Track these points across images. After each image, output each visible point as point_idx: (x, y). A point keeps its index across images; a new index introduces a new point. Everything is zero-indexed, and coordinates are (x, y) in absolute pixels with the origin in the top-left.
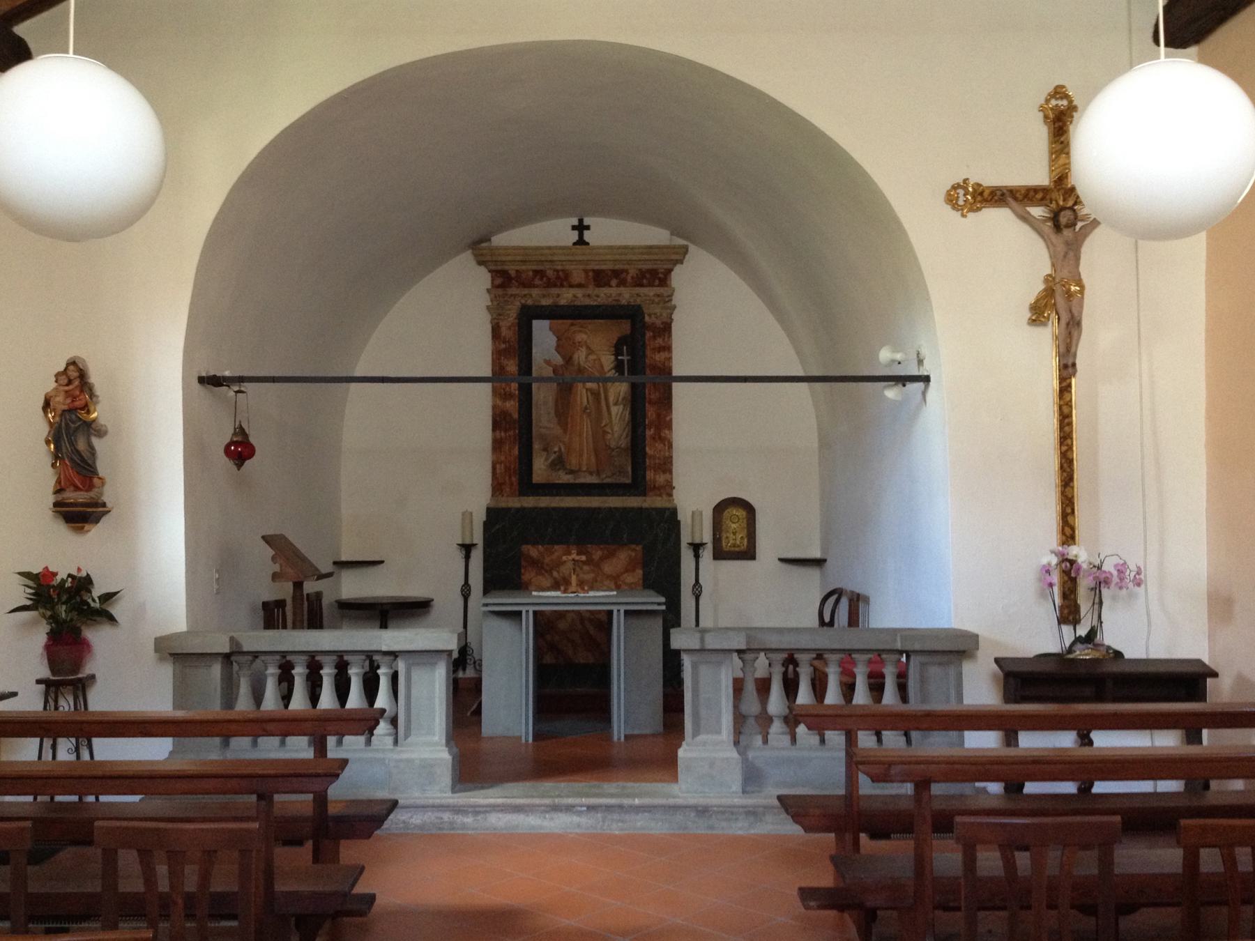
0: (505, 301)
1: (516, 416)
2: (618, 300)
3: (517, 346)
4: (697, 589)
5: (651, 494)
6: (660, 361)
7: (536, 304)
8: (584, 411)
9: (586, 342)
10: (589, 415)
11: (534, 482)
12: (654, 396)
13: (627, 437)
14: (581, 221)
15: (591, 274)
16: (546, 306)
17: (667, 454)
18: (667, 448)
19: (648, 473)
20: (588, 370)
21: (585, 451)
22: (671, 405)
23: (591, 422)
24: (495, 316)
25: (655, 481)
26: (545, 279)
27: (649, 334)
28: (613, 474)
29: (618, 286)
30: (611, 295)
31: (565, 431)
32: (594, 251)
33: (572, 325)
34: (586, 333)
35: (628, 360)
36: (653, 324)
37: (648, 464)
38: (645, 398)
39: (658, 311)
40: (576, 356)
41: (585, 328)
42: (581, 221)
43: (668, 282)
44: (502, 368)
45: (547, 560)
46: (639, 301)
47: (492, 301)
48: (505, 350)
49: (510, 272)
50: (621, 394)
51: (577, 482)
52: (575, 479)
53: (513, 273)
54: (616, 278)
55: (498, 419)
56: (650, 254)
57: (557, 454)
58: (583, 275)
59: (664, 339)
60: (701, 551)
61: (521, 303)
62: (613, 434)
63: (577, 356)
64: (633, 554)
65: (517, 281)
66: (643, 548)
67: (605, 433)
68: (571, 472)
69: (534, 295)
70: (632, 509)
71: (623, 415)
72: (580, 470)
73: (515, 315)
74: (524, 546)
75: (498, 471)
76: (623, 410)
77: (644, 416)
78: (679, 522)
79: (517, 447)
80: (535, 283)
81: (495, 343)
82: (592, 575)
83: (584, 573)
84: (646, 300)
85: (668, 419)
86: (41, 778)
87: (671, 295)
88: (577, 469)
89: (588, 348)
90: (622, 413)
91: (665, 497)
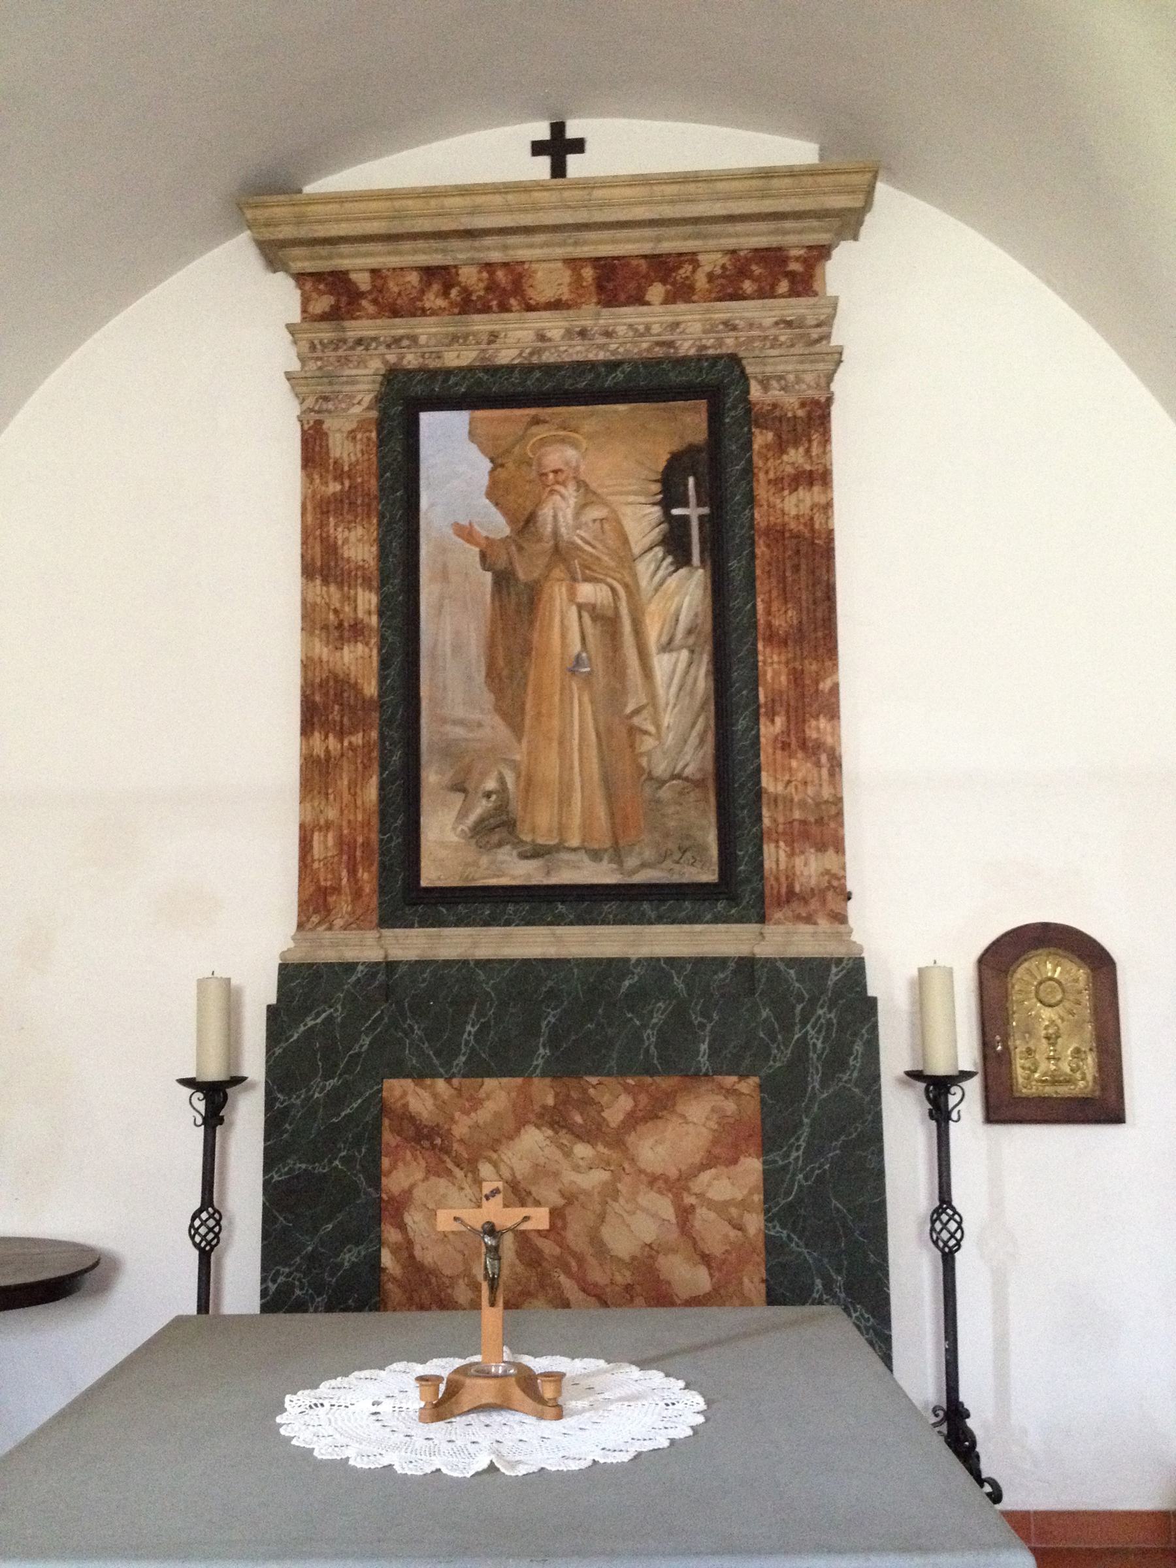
0: (339, 359)
1: (371, 689)
2: (670, 344)
3: (373, 485)
4: (945, 1226)
5: (778, 915)
6: (797, 517)
7: (433, 364)
8: (573, 672)
9: (576, 469)
10: (588, 679)
11: (424, 883)
12: (784, 619)
13: (702, 741)
14: (558, 129)
15: (588, 273)
16: (460, 369)
17: (826, 793)
18: (825, 772)
19: (768, 849)
20: (584, 551)
21: (578, 785)
22: (835, 647)
23: (592, 702)
24: (310, 402)
25: (791, 877)
26: (454, 292)
27: (762, 439)
28: (665, 856)
29: (669, 299)
30: (648, 328)
31: (517, 729)
32: (598, 193)
33: (536, 421)
34: (575, 445)
35: (701, 518)
36: (775, 406)
37: (766, 822)
38: (754, 625)
39: (787, 367)
40: (546, 512)
41: (575, 431)
42: (558, 129)
43: (816, 287)
44: (331, 549)
45: (461, 1128)
46: (730, 344)
47: (302, 359)
48: (338, 499)
49: (353, 276)
50: (682, 618)
51: (553, 881)
52: (548, 873)
53: (363, 281)
54: (664, 281)
55: (317, 698)
56: (764, 195)
57: (494, 797)
58: (566, 276)
59: (808, 451)
60: (952, 1100)
61: (385, 362)
62: (659, 736)
63: (551, 513)
64: (730, 1106)
65: (375, 302)
66: (761, 1087)
67: (634, 732)
68: (537, 852)
69: (423, 339)
70: (721, 962)
71: (690, 680)
72: (559, 847)
73: (368, 399)
74: (388, 1083)
75: (317, 850)
76: (690, 664)
77: (754, 682)
78: (873, 1002)
79: (374, 781)
80: (427, 305)
81: (312, 481)
82: (599, 1176)
83: (576, 1168)
84: (752, 339)
85: (825, 686)
86: (229, 1050)
87: (827, 322)
88: (553, 842)
89: (581, 484)
90: (686, 672)
91: (824, 924)
